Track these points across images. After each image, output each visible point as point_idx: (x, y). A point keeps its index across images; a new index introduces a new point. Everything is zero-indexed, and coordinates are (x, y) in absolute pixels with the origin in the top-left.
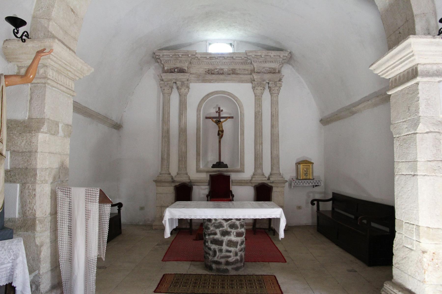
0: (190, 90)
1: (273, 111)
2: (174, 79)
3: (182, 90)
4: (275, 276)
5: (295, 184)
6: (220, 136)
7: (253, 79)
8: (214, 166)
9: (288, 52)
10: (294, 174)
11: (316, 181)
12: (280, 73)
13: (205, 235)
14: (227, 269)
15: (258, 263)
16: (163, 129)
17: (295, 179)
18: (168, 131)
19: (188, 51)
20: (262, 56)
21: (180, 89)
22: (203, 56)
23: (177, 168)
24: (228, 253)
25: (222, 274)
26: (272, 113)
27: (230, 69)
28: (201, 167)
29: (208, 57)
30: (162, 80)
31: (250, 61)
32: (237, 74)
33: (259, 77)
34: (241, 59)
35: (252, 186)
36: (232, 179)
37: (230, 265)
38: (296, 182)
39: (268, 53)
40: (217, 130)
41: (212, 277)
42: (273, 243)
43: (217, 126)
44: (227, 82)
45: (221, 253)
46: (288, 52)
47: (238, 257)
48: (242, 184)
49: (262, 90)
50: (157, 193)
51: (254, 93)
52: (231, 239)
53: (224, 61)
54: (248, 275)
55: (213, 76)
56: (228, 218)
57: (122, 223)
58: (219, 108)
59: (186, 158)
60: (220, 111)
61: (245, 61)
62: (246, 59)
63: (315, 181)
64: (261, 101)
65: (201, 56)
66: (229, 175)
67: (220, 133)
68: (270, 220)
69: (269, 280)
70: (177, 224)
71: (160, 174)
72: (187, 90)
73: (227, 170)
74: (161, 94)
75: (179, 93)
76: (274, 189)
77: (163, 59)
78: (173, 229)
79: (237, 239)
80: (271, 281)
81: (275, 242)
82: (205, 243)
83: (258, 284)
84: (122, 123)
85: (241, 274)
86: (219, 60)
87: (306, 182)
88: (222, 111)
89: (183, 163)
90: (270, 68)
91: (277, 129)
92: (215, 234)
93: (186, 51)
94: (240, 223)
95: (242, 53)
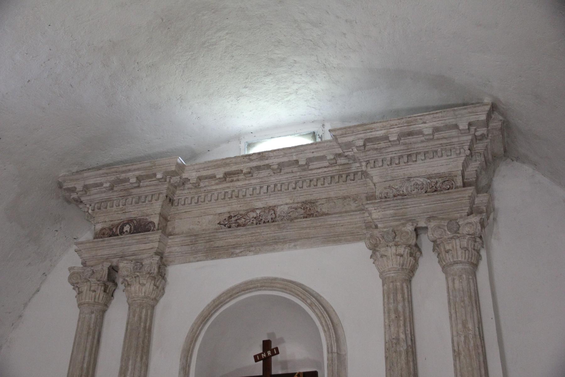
3: (133, 288)
27: (295, 205)
39: (409, 123)
49: (402, 256)
53: (274, 179)
77: (89, 198)
86: (258, 181)
88: (273, 354)
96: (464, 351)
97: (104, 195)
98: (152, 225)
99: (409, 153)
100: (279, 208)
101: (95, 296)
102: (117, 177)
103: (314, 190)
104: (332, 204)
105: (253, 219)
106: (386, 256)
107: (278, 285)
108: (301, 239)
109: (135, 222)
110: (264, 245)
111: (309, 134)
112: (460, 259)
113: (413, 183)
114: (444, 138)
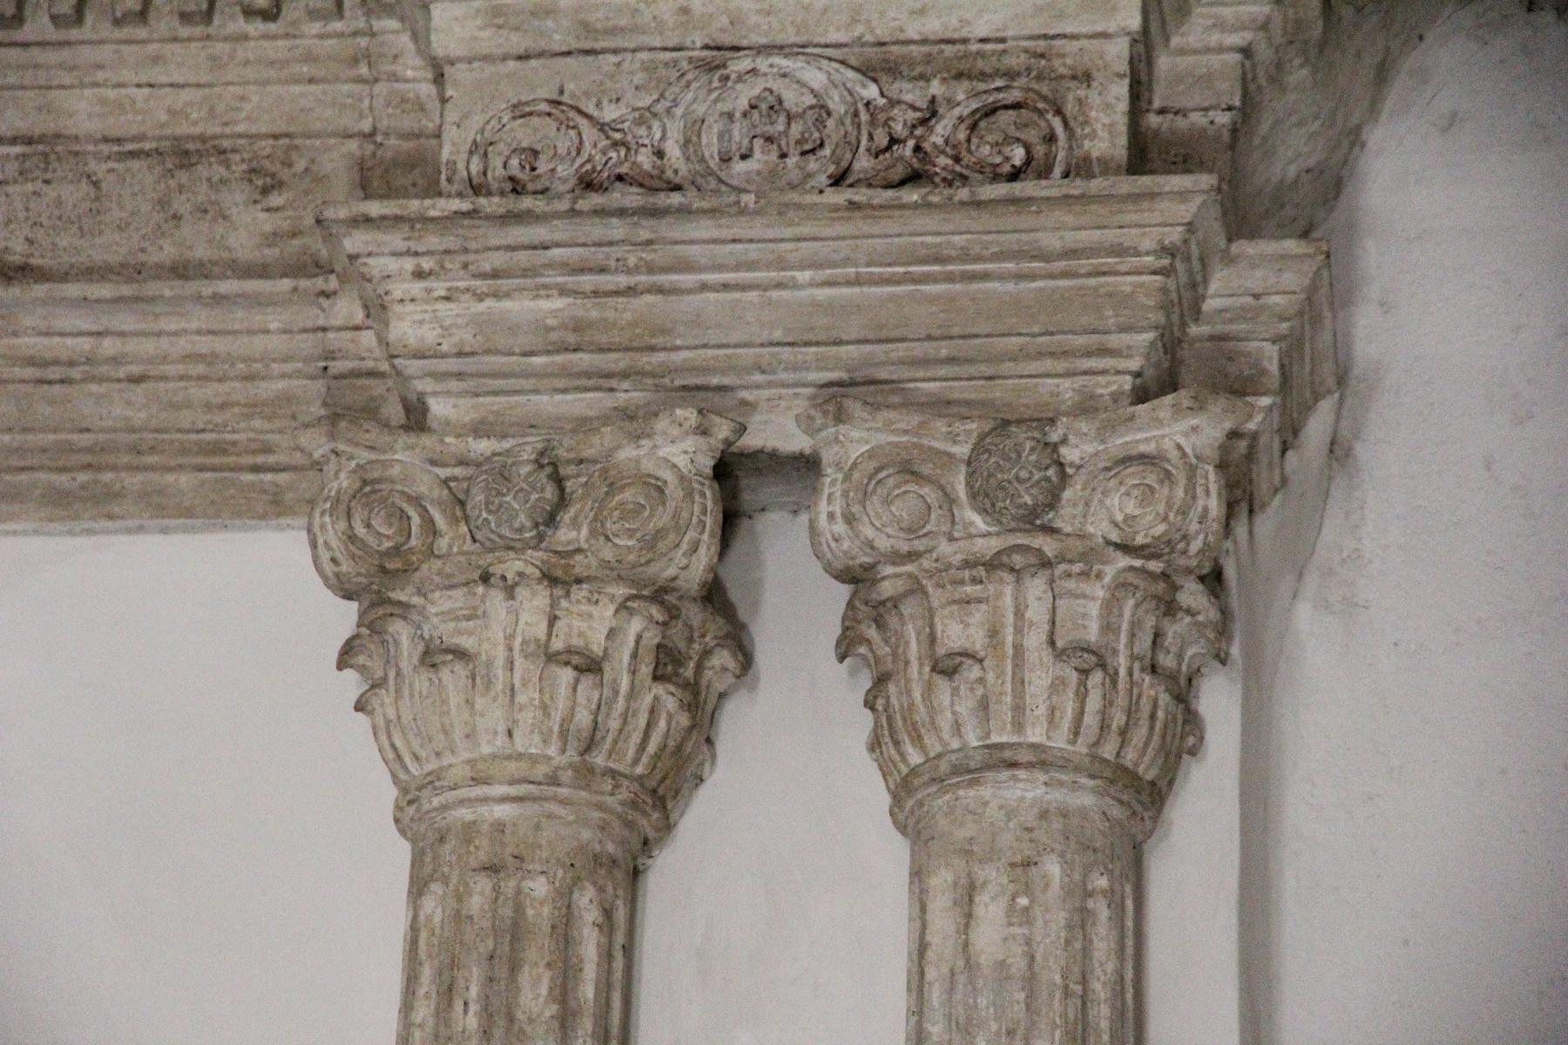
33: (520, 307)
49: (590, 666)
104: (73, 194)
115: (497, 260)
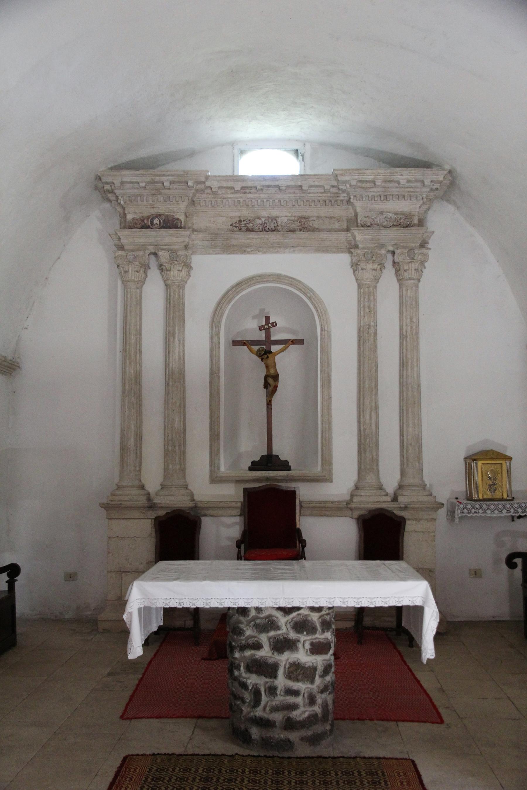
0: (192, 273)
1: (404, 324)
2: (151, 244)
3: (172, 273)
4: (413, 762)
5: (463, 513)
6: (271, 388)
7: (353, 244)
8: (255, 466)
9: (444, 170)
10: (461, 487)
11: (520, 504)
12: (422, 226)
13: (232, 649)
14: (289, 740)
15: (368, 722)
16: (124, 372)
17: (465, 497)
18: (138, 379)
19: (186, 173)
20: (377, 184)
21: (167, 270)
22: (225, 184)
23: (161, 471)
24: (291, 697)
25: (276, 754)
26: (401, 329)
27: (293, 218)
28: (222, 469)
29: (237, 188)
30: (121, 248)
31: (345, 195)
32: (314, 230)
33: (367, 237)
34: (322, 190)
35: (352, 518)
36: (301, 499)
37: (297, 729)
38: (466, 508)
40: (263, 374)
41: (249, 762)
42: (408, 666)
43: (263, 365)
44: (288, 250)
45: (272, 698)
46: (444, 170)
47: (317, 709)
48: (327, 513)
50: (109, 538)
51: (357, 280)
52: (298, 659)
53: (279, 196)
54: (343, 757)
55: (252, 235)
56: (290, 606)
57: (17, 615)
58: (267, 318)
59: (184, 446)
60: (270, 325)
61: (332, 195)
62: (335, 190)
63: (516, 505)
64: (375, 300)
65: (219, 185)
66: (293, 489)
67: (270, 381)
68: (399, 610)
69: (399, 774)
70: (159, 620)
71: (119, 487)
72: (186, 273)
73: (287, 477)
74: (119, 282)
75: (165, 281)
76: (410, 526)
77: (121, 191)
78: (150, 632)
79: (314, 661)
80: (405, 774)
81: (412, 666)
82: (231, 672)
83: (368, 783)
84: (19, 358)
85: (325, 754)
86: (266, 195)
87: (492, 507)
88: (273, 326)
89: (177, 460)
90: (396, 214)
91: (415, 369)
92: (258, 646)
93: (181, 173)
94: (320, 617)
95: (326, 175)
96: (410, 335)
97: (136, 191)
98: (179, 222)
99: (385, 194)
100: (280, 218)
101: (139, 275)
102: (152, 179)
103: (308, 208)
104: (321, 221)
105: (259, 225)
106: (365, 269)
107: (286, 281)
108: (298, 246)
109: (163, 217)
110: (270, 247)
111: (292, 150)
112: (413, 277)
113: (385, 216)
114: (412, 187)
115: (366, 233)
